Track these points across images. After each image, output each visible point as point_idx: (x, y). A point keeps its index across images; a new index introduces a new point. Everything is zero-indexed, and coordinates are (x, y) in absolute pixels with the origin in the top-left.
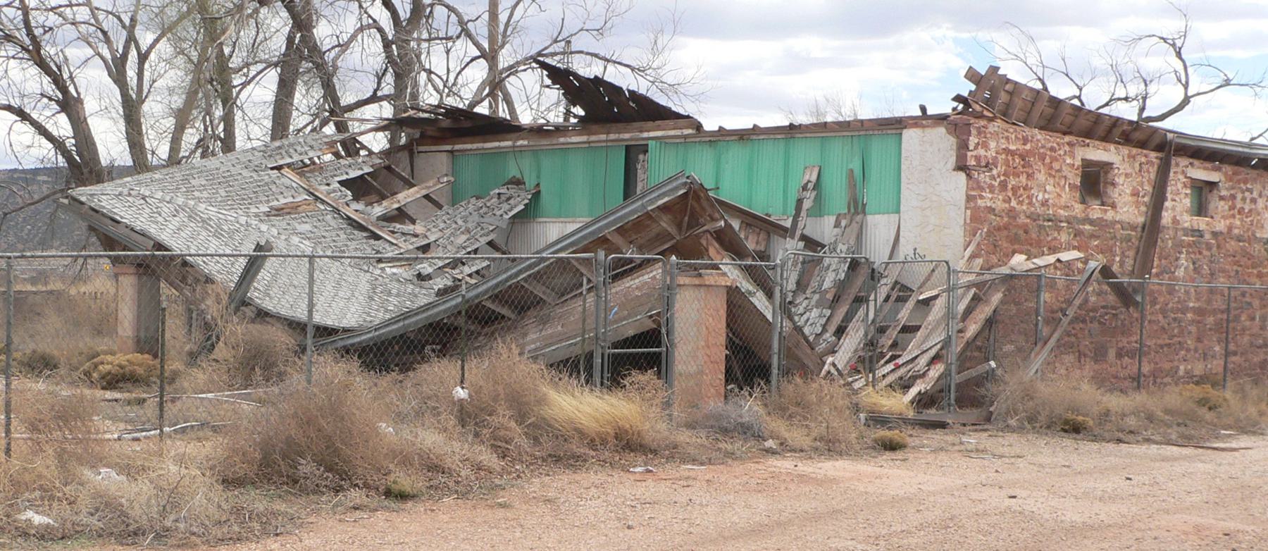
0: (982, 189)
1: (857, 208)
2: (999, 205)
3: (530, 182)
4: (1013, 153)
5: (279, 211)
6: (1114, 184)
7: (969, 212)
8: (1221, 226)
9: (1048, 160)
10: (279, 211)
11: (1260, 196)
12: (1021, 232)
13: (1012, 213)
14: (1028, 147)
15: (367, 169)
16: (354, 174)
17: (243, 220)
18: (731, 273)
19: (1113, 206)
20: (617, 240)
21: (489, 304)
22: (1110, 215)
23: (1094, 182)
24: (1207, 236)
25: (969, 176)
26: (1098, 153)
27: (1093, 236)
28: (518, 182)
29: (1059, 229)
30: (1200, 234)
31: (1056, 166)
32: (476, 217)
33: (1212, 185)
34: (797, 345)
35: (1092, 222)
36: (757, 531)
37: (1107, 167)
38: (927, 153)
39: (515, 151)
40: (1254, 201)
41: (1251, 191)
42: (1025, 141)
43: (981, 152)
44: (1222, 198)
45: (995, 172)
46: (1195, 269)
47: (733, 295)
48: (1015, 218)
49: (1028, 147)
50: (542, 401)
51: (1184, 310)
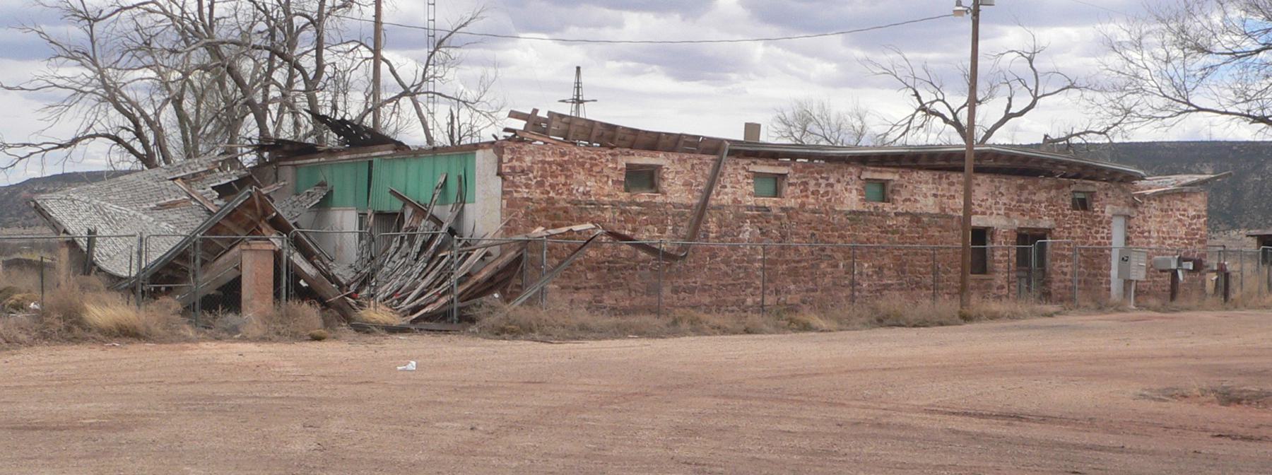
0: (518, 186)
1: (462, 200)
2: (537, 194)
3: (329, 187)
4: (550, 163)
5: (162, 207)
6: (663, 179)
7: (505, 202)
8: (791, 203)
9: (587, 166)
10: (162, 207)
11: (839, 181)
12: (561, 213)
13: (551, 201)
14: (566, 158)
15: (234, 178)
16: (223, 182)
17: (132, 213)
18: (277, 241)
19: (664, 193)
20: (228, 224)
21: (176, 262)
22: (659, 199)
23: (644, 178)
24: (774, 211)
25: (504, 179)
26: (643, 159)
27: (639, 213)
28: (322, 185)
29: (603, 210)
30: (768, 209)
31: (596, 169)
32: (290, 208)
33: (784, 176)
34: (323, 283)
35: (639, 204)
36: (903, 466)
37: (659, 167)
38: (484, 162)
39: (319, 165)
40: (832, 185)
41: (827, 179)
42: (563, 154)
43: (515, 163)
44: (790, 184)
45: (531, 175)
46: (762, 234)
47: (277, 255)
48: (553, 204)
49: (566, 158)
50: (85, 310)
51: (751, 261)
